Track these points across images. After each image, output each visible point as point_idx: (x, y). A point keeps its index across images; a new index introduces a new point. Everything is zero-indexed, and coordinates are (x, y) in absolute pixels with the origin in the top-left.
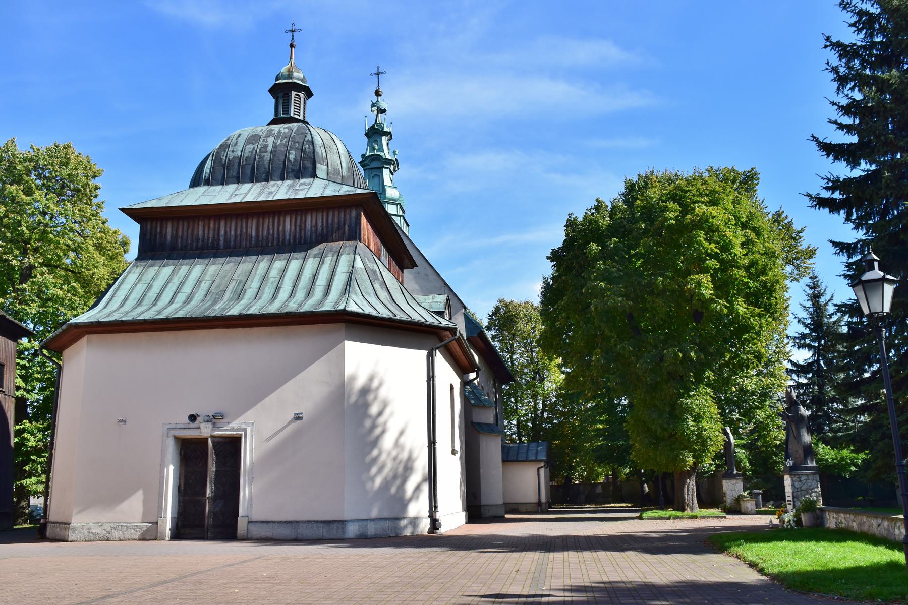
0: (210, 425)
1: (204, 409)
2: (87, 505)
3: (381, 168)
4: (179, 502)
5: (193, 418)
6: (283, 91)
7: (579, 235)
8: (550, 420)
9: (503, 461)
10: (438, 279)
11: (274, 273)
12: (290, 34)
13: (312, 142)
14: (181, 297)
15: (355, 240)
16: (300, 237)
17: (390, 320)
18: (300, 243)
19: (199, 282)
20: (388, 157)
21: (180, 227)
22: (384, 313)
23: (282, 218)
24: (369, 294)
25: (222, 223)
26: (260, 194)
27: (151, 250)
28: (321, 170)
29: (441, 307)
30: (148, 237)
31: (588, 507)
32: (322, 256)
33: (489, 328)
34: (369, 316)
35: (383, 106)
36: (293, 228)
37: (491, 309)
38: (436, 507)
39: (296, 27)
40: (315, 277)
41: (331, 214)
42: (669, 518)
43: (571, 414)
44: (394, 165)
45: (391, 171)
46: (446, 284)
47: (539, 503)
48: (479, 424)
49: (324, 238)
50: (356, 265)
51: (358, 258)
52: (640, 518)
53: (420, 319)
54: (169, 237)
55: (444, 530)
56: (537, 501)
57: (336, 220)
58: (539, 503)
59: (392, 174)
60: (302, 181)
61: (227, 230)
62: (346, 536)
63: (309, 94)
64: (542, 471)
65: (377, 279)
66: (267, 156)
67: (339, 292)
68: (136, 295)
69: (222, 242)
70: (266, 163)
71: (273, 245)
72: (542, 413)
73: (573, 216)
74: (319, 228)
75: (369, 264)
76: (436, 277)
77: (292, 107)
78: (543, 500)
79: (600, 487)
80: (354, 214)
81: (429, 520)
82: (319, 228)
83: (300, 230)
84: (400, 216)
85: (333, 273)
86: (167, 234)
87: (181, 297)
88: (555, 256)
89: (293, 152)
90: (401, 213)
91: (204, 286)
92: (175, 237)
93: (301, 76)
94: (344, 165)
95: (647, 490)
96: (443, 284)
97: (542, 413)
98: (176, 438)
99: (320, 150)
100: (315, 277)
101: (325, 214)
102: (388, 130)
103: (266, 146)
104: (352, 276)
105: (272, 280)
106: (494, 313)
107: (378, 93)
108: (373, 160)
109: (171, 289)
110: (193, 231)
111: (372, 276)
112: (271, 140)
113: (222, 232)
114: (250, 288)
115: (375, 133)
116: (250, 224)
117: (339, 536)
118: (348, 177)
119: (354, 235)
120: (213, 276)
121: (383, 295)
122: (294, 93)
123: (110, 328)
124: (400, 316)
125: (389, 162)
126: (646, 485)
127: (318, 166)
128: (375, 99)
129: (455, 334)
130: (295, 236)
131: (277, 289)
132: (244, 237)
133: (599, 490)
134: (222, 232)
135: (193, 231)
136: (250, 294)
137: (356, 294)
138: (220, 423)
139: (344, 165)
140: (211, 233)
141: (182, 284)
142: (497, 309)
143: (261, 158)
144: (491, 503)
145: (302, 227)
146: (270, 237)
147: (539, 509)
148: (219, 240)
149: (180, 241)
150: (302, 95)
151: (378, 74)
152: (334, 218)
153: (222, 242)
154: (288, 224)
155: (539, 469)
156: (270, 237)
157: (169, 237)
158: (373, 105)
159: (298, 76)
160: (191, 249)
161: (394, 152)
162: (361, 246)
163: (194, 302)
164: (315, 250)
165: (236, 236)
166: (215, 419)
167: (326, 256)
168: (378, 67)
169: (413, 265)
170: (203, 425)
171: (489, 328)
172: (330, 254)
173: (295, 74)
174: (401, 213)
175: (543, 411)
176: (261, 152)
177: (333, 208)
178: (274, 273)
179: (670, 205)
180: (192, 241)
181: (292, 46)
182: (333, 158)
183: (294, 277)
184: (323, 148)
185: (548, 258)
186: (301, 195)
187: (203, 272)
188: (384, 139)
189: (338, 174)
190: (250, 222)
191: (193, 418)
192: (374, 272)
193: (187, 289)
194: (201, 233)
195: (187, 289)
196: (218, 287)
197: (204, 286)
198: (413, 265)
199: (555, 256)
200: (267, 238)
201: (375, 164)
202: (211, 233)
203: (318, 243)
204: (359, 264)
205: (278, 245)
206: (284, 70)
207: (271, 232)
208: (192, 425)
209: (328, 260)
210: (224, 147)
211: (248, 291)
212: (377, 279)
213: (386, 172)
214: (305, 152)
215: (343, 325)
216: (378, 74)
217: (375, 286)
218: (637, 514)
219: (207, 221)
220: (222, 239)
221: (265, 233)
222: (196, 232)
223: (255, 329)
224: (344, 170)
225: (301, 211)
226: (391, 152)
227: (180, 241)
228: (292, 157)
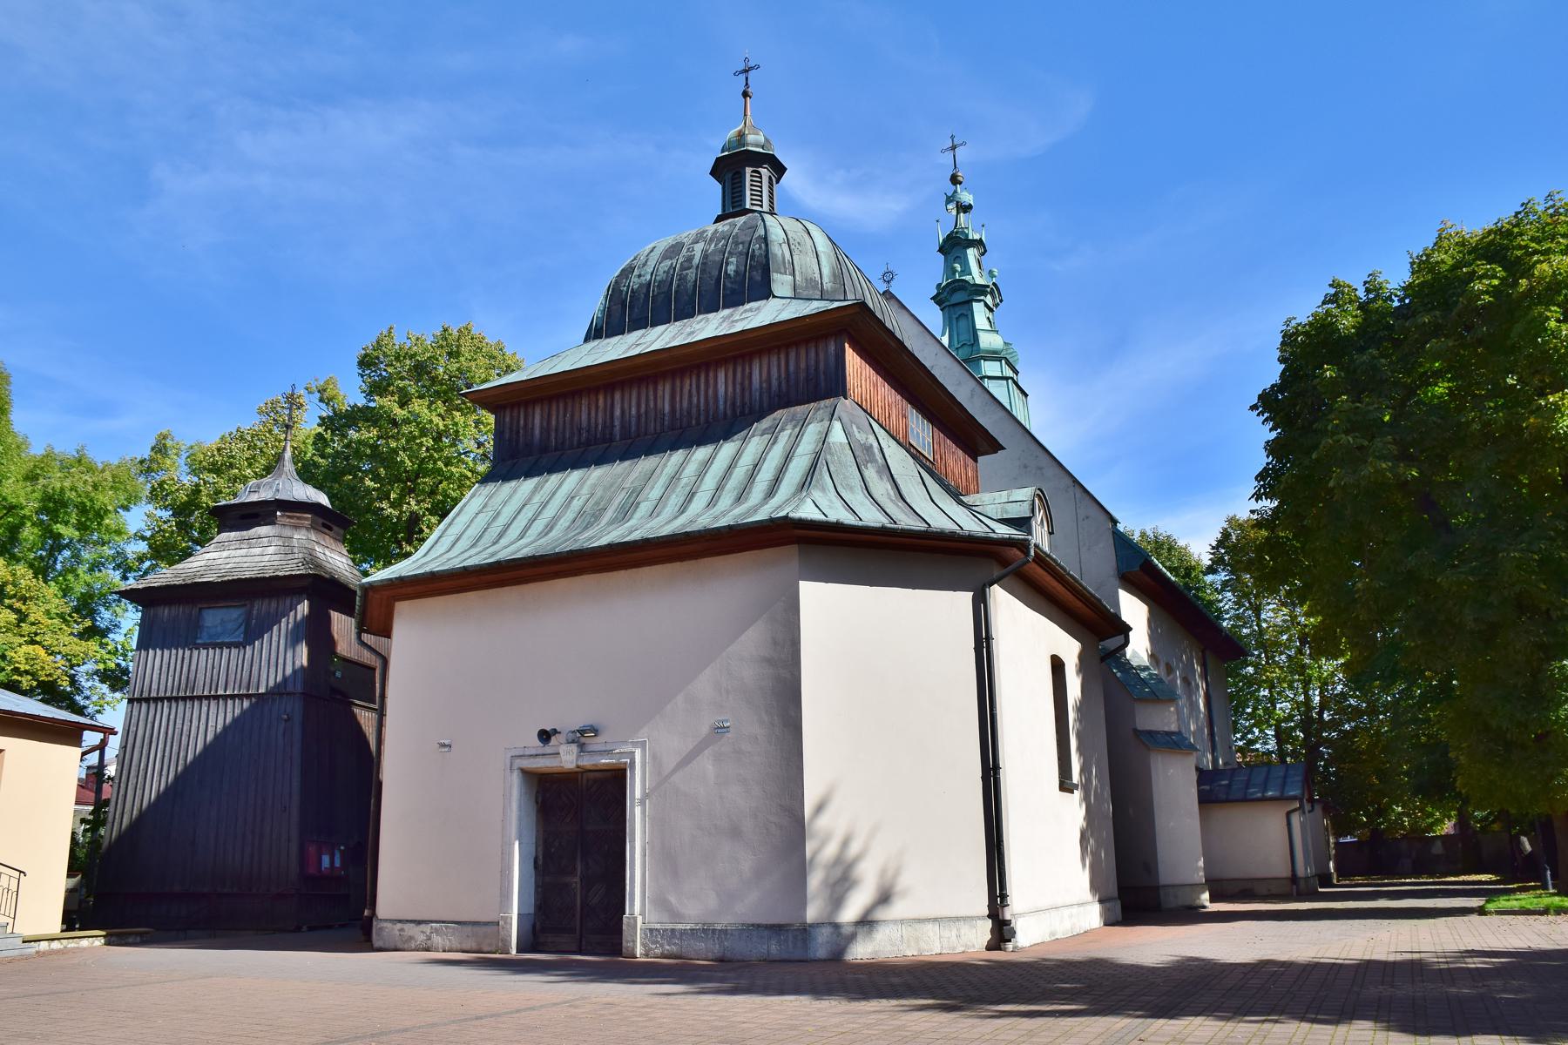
0: (574, 747)
1: (567, 719)
2: (802, 903)
3: (969, 303)
4: (537, 886)
5: (545, 736)
6: (734, 168)
7: (1307, 349)
8: (1333, 724)
9: (1200, 802)
10: (1062, 473)
11: (691, 469)
12: (743, 77)
13: (765, 239)
14: (539, 526)
15: (837, 396)
16: (743, 404)
17: (882, 531)
18: (742, 414)
19: (571, 498)
20: (979, 281)
21: (554, 413)
22: (871, 517)
23: (711, 374)
24: (851, 489)
25: (618, 396)
26: (674, 338)
27: (515, 459)
28: (781, 283)
29: (1020, 511)
30: (507, 436)
31: (1408, 884)
32: (773, 432)
33: (1211, 570)
34: (838, 527)
35: (966, 197)
36: (730, 389)
37: (1214, 536)
38: (1004, 896)
39: (751, 64)
40: (756, 467)
41: (793, 355)
42: (1545, 912)
43: (1373, 711)
44: (992, 293)
45: (986, 305)
46: (1076, 481)
47: (1294, 878)
48: (1150, 733)
49: (784, 400)
50: (831, 439)
51: (837, 426)
52: (1481, 911)
53: (948, 526)
54: (537, 432)
55: (1033, 933)
56: (1286, 873)
57: (803, 365)
58: (1294, 878)
59: (991, 310)
60: (747, 306)
61: (625, 407)
62: (811, 956)
63: (779, 169)
64: (1296, 820)
65: (873, 460)
66: (691, 274)
67: (793, 490)
68: (473, 531)
69: (617, 428)
70: (690, 285)
71: (698, 423)
72: (1320, 714)
73: (1293, 323)
74: (775, 382)
75: (859, 436)
76: (1058, 470)
77: (748, 193)
78: (1301, 872)
79: (1439, 843)
80: (832, 348)
81: (989, 923)
82: (775, 382)
83: (743, 390)
84: (1006, 379)
85: (788, 458)
86: (546, 426)
87: (539, 526)
88: (1268, 403)
89: (733, 259)
90: (1010, 373)
91: (577, 504)
92: (546, 430)
93: (761, 139)
94: (826, 271)
95: (1528, 848)
96: (1069, 481)
97: (1320, 714)
98: (527, 774)
99: (779, 250)
100: (756, 467)
101: (783, 357)
102: (977, 237)
103: (690, 259)
104: (849, 459)
105: (684, 481)
106: (1220, 543)
107: (954, 180)
108: (954, 291)
109: (528, 512)
110: (572, 416)
111: (862, 456)
112: (699, 248)
113: (618, 412)
114: (647, 499)
115: (954, 245)
116: (660, 393)
117: (798, 954)
118: (834, 291)
119: (835, 386)
120: (594, 486)
121: (881, 488)
122: (748, 170)
123: (409, 590)
124: (906, 522)
125: (981, 290)
126: (1524, 839)
127: (775, 276)
128: (950, 188)
129: (1027, 553)
130: (734, 404)
131: (691, 496)
132: (652, 415)
133: (1438, 849)
134: (618, 412)
135: (572, 416)
136: (644, 508)
137: (823, 490)
138: (596, 744)
139: (826, 271)
140: (600, 414)
141: (544, 505)
142: (1226, 535)
143: (682, 278)
144: (1177, 882)
145: (746, 387)
146: (694, 410)
147: (1294, 892)
148: (613, 426)
149: (553, 435)
150: (764, 171)
151: (953, 148)
152: (800, 360)
153: (617, 428)
154: (722, 383)
155: (1288, 814)
156: (694, 410)
157: (537, 432)
158: (949, 200)
159: (755, 141)
160: (571, 448)
161: (991, 272)
162: (844, 405)
163: (553, 534)
164: (766, 423)
165: (639, 416)
166: (582, 736)
167: (783, 430)
168: (952, 137)
169: (995, 446)
170: (563, 749)
171: (1211, 570)
172: (789, 427)
173: (750, 138)
174: (1010, 373)
175: (1323, 706)
176: (683, 268)
177: (797, 344)
178: (691, 469)
179: (1483, 267)
180: (572, 434)
181: (745, 94)
182: (804, 262)
183: (721, 474)
184: (785, 247)
185: (1253, 408)
186: (738, 328)
187: (582, 482)
188: (972, 253)
189: (815, 287)
190: (660, 388)
191: (545, 736)
192: (869, 449)
193: (549, 513)
194: (584, 417)
195: (549, 513)
196: (597, 503)
197: (577, 504)
198: (995, 446)
199: (1268, 403)
200: (689, 413)
201: (959, 297)
202: (600, 414)
203: (772, 410)
204: (837, 435)
205: (707, 421)
206: (733, 133)
207: (695, 400)
208: (548, 750)
209: (784, 438)
210: (627, 272)
211: (643, 506)
212: (873, 460)
213: (978, 308)
214: (753, 256)
215: (793, 549)
216: (953, 148)
217: (866, 473)
218: (1475, 902)
219: (593, 397)
220: (617, 423)
221: (685, 404)
222: (576, 418)
223: (646, 569)
224: (826, 280)
225: (742, 356)
226: (985, 274)
227: (553, 435)
228: (731, 269)
